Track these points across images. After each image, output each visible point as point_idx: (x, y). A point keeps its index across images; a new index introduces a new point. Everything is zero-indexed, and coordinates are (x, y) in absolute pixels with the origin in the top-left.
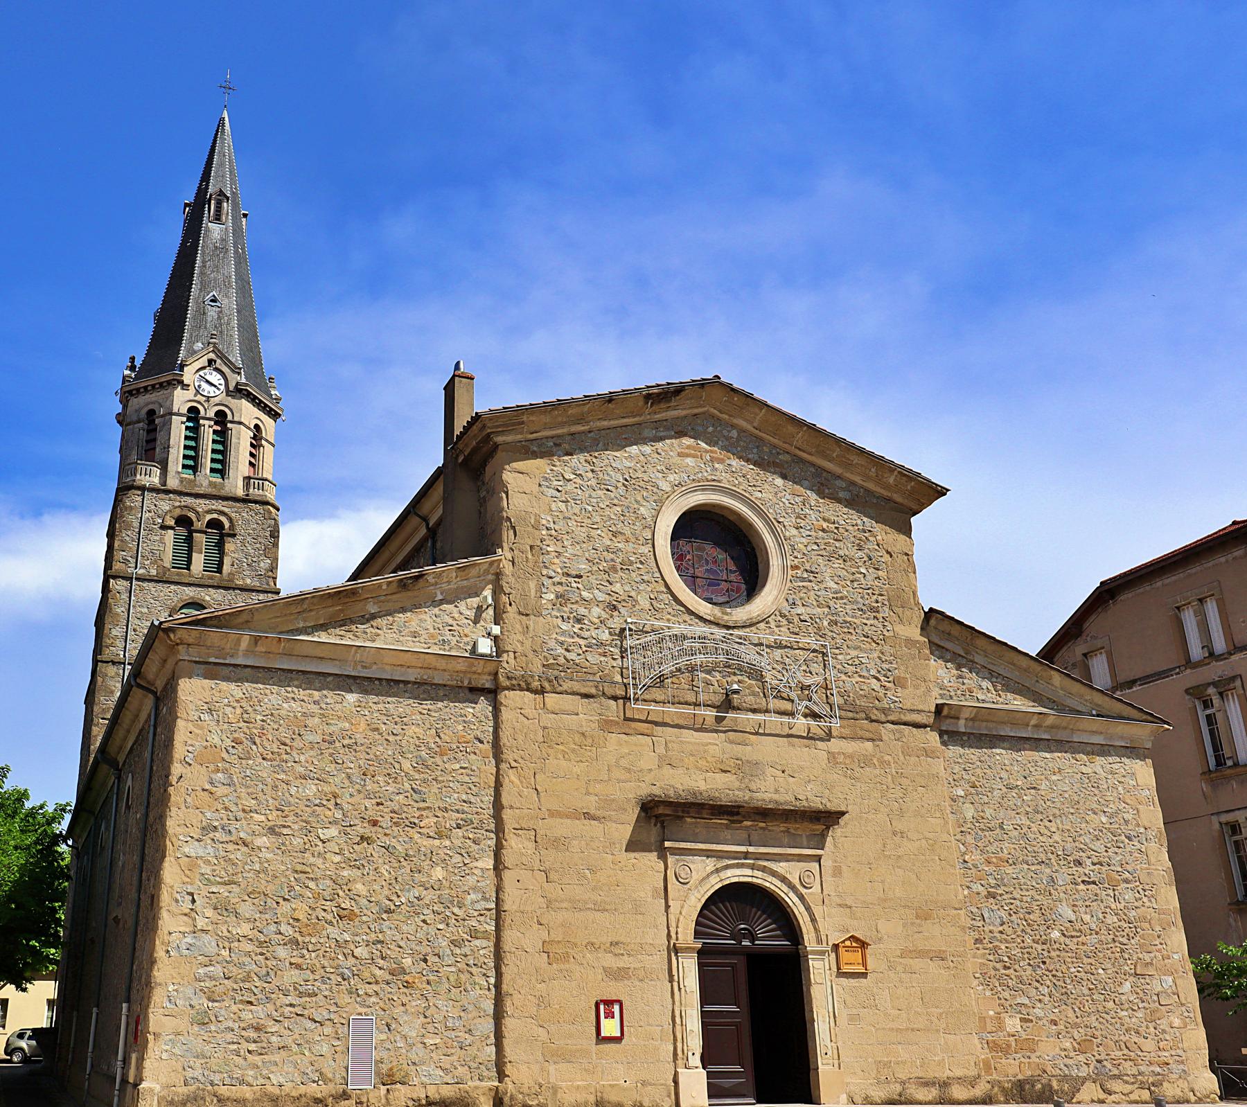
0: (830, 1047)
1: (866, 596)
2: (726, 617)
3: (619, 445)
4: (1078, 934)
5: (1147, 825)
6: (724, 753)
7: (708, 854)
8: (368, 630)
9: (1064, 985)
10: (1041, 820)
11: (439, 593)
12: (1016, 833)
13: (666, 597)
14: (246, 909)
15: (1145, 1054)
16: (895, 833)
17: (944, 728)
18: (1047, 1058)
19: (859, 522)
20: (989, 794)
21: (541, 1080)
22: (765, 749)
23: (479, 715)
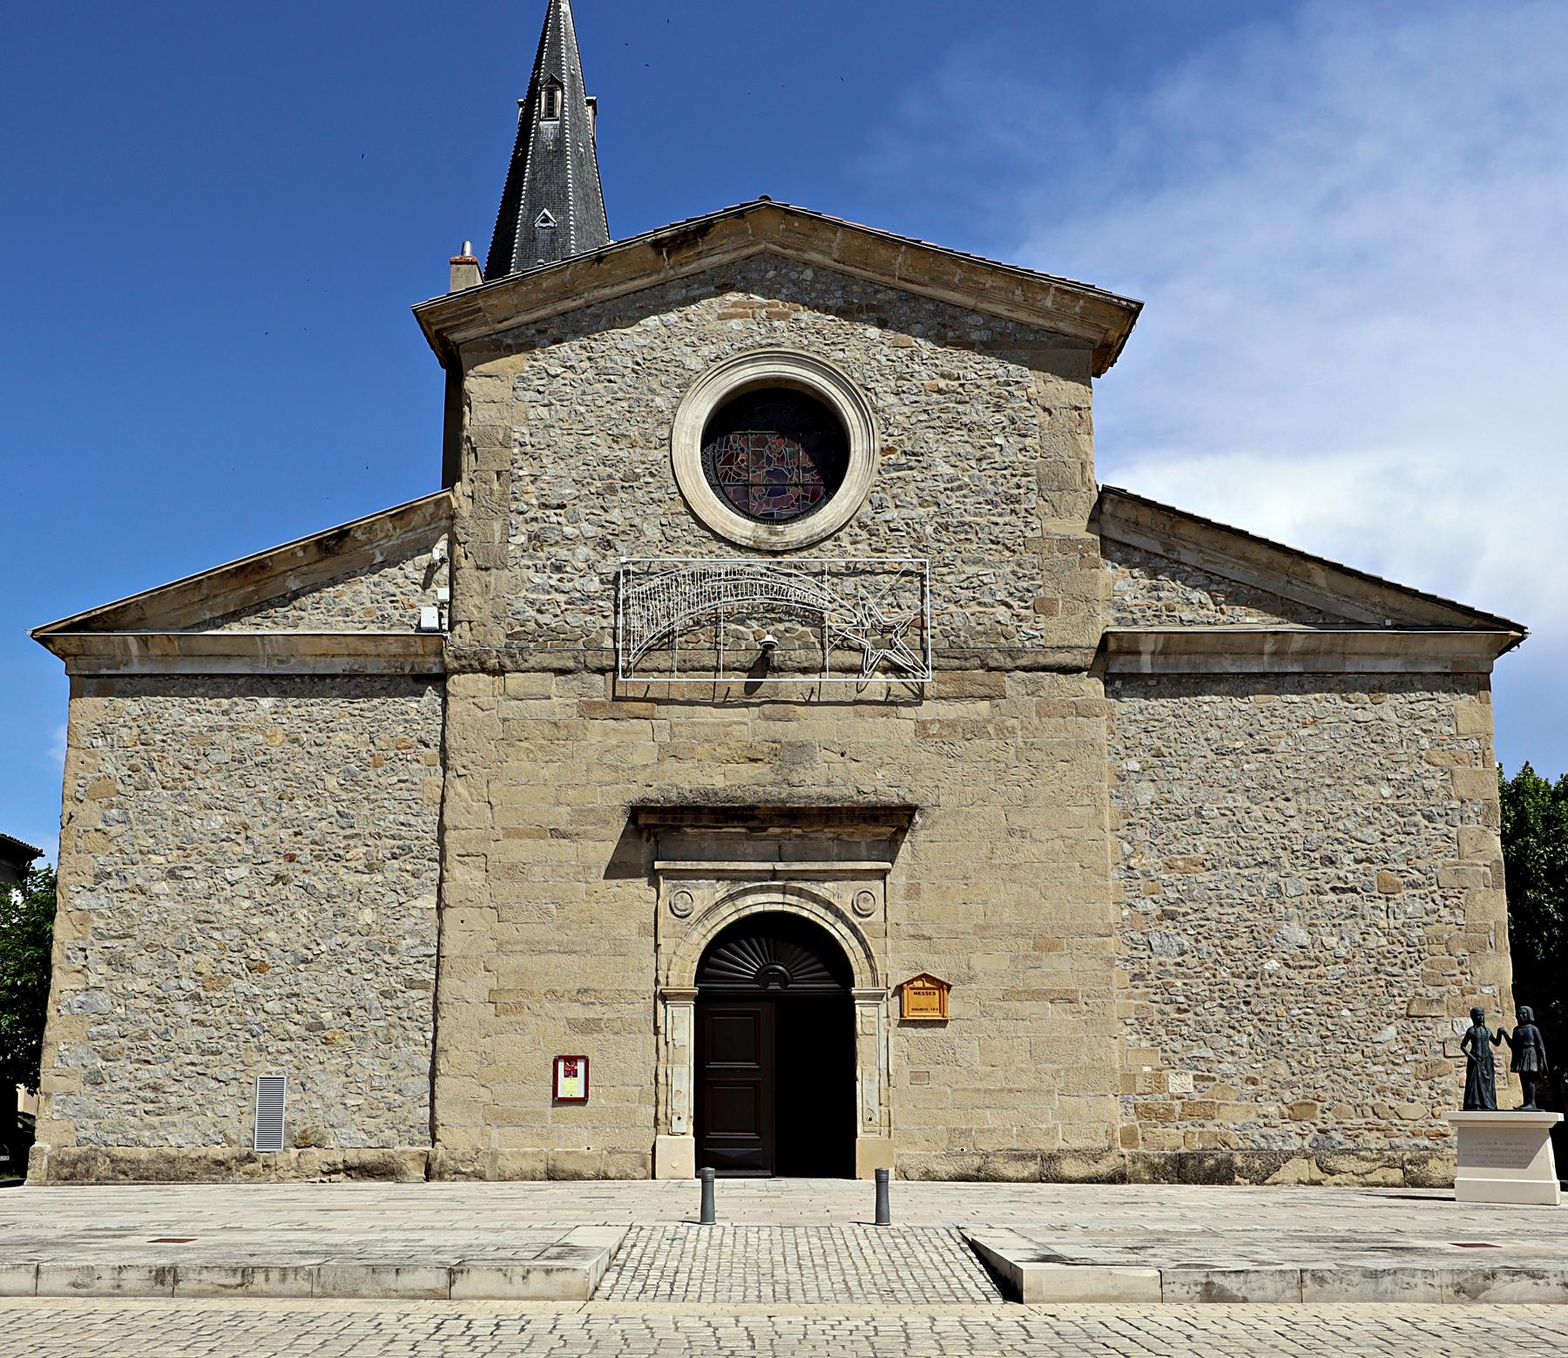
0: (876, 1111)
1: (1001, 480)
2: (774, 539)
3: (630, 318)
4: (1313, 964)
5: (1464, 793)
6: (755, 734)
7: (719, 876)
8: (289, 614)
9: (1276, 1032)
10: (1272, 799)
11: (378, 553)
12: (1223, 821)
14: (143, 963)
15: (1405, 1122)
16: (1011, 832)
17: (1114, 670)
18: (1232, 1126)
19: (1000, 371)
20: (1184, 765)
21: (479, 1146)
22: (818, 725)
23: (425, 710)
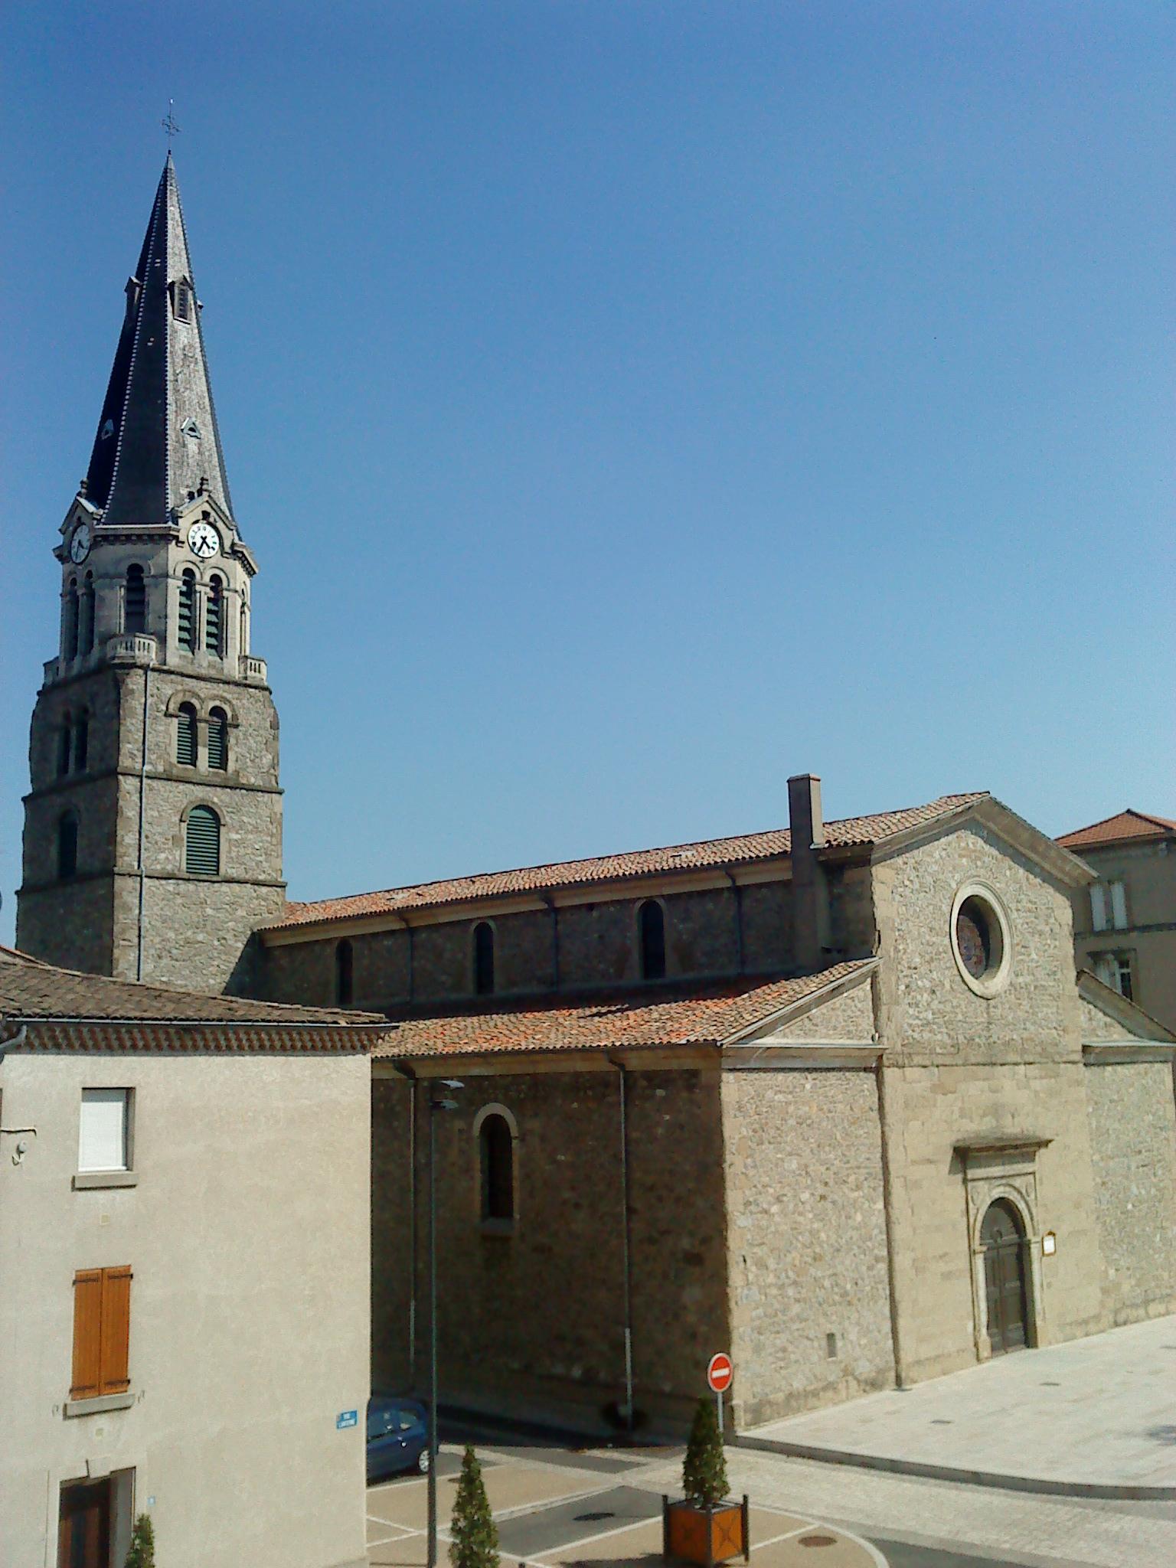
13: (959, 978)
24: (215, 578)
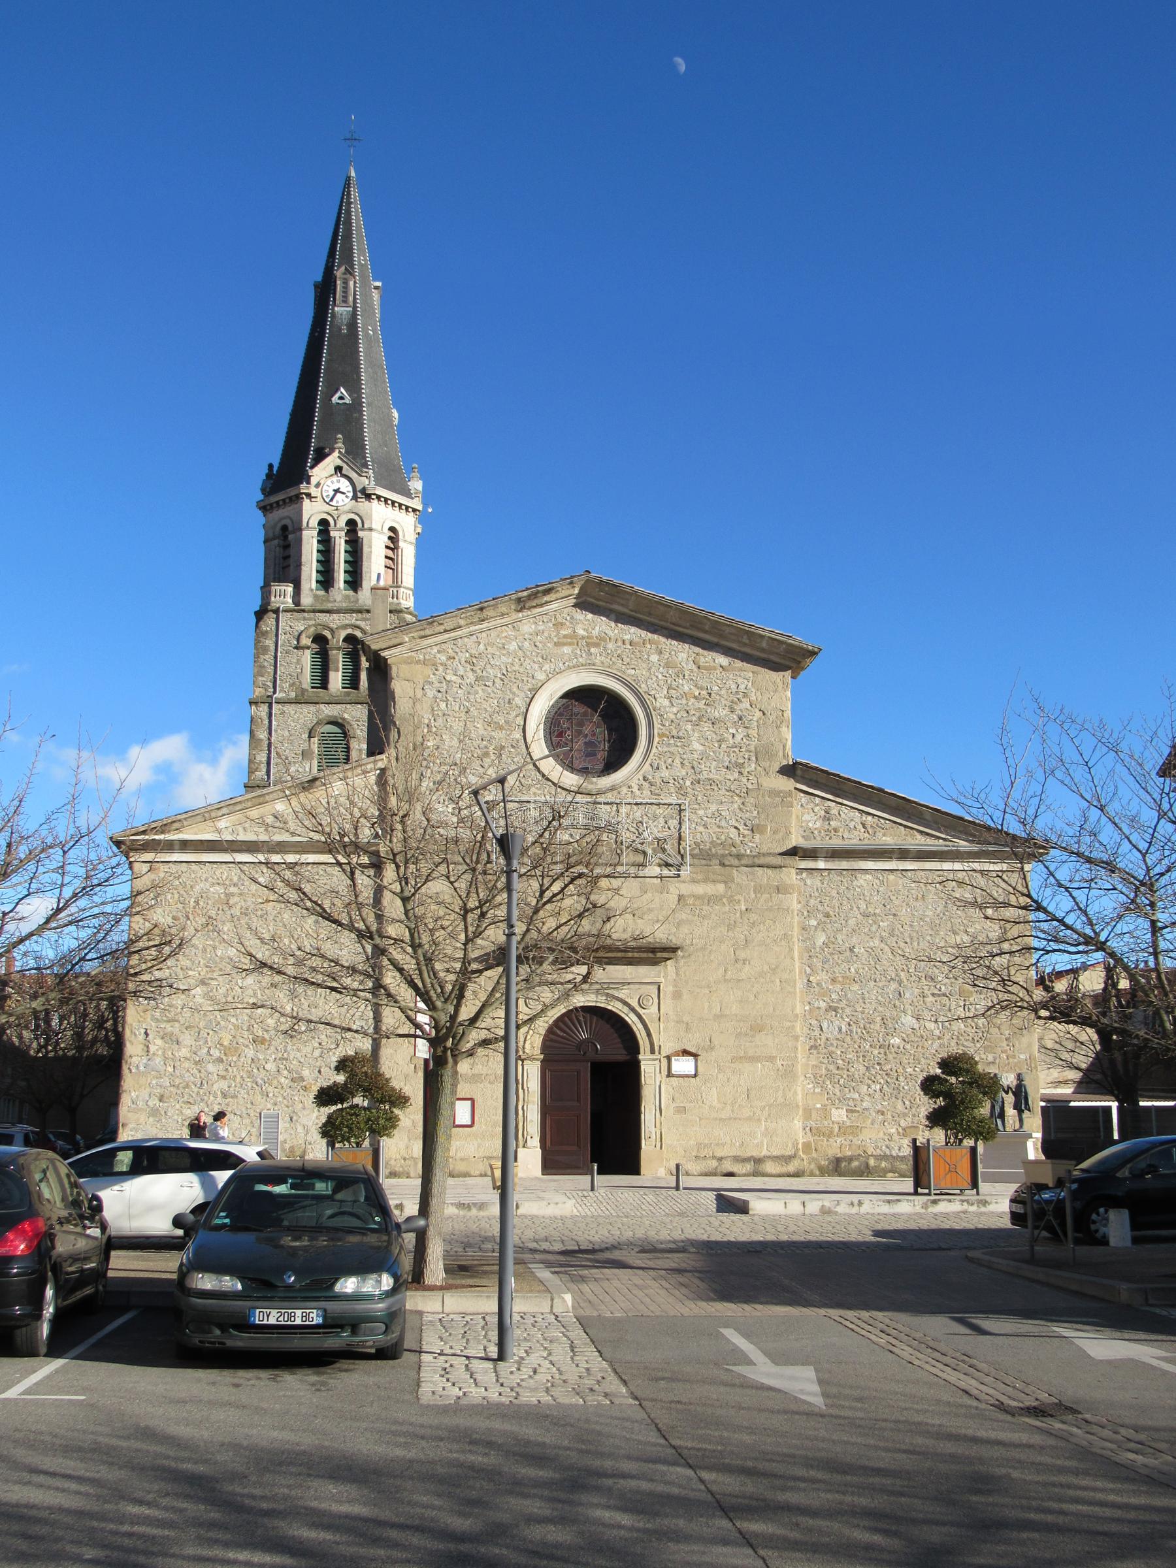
24: (351, 523)
